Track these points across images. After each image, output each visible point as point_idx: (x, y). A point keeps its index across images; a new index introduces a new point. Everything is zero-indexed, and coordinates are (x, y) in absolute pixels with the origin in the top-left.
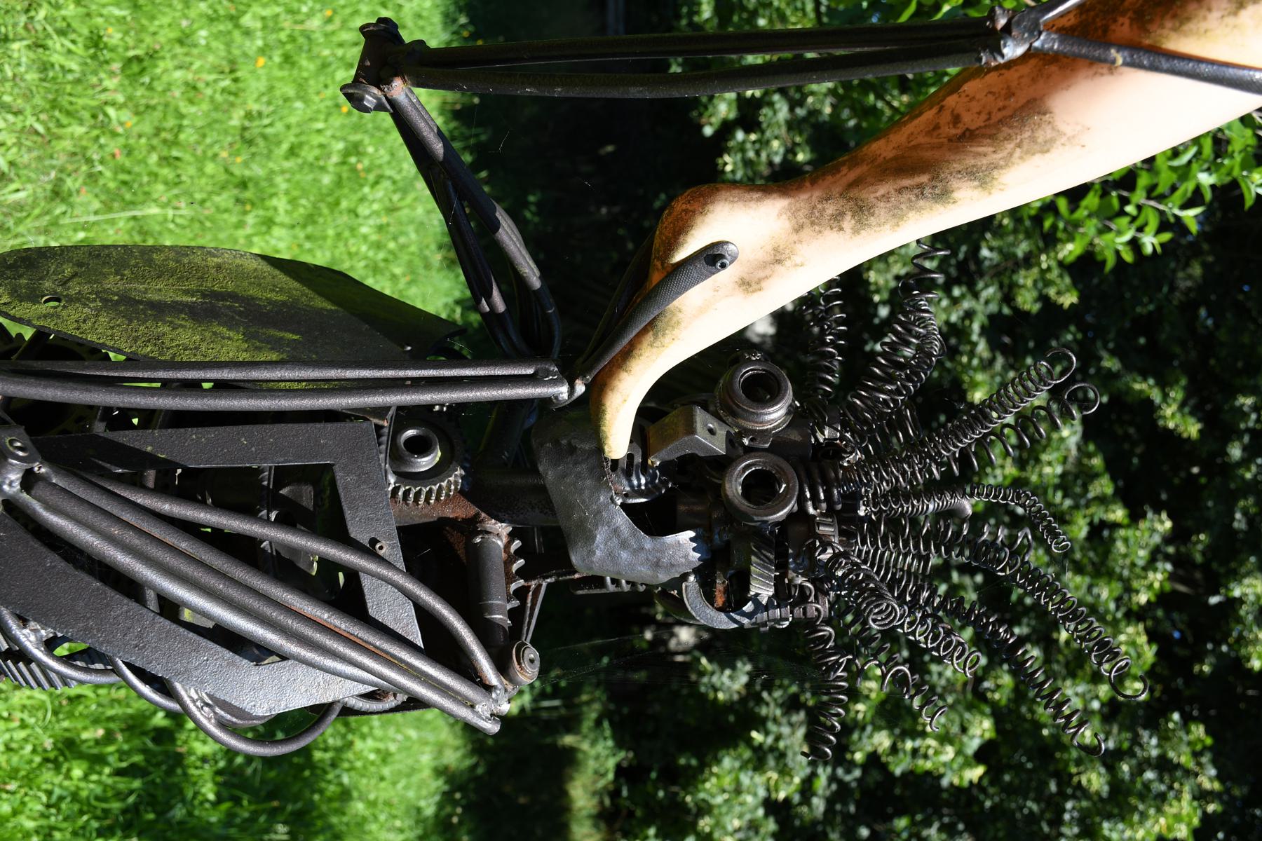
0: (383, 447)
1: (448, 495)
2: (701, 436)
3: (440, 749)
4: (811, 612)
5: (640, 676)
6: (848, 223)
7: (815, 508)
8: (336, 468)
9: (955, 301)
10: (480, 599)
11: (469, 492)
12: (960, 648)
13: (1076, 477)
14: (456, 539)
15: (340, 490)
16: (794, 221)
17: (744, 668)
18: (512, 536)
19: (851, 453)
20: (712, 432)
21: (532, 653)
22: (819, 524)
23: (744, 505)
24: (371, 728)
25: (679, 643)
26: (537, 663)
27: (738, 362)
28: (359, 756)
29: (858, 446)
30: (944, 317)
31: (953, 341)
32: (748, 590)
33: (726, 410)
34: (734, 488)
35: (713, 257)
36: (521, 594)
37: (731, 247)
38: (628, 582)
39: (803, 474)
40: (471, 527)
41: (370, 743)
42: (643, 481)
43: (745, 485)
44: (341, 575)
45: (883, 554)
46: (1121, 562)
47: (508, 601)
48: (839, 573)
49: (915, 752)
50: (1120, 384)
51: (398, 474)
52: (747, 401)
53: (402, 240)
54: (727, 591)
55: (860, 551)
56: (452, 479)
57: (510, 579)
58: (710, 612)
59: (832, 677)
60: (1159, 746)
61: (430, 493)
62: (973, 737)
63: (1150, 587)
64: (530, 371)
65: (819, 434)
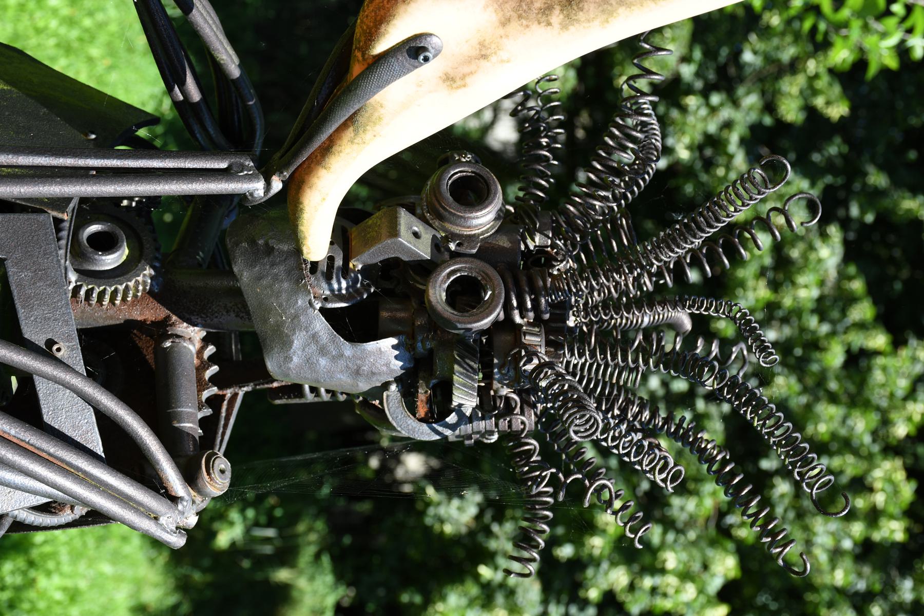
0: (63, 242)
1: (135, 296)
2: (405, 239)
3: (138, 584)
4: (517, 426)
5: (365, 507)
6: (556, 17)
7: (522, 317)
8: (8, 263)
9: (713, 110)
10: (170, 407)
11: (161, 293)
12: (662, 461)
13: (835, 300)
14: (144, 344)
15: (13, 287)
16: (500, 14)
17: (472, 501)
18: (206, 341)
19: (562, 261)
20: (416, 235)
21: (222, 463)
22: (525, 334)
23: (448, 312)
24: (58, 563)
25: (407, 472)
26: (228, 474)
27: (447, 162)
28: (43, 594)
29: (567, 254)
30: (700, 126)
31: (708, 152)
32: (451, 401)
33: (432, 213)
34: (437, 293)
35: (415, 50)
36: (214, 402)
37: (434, 40)
38: (328, 391)
39: (510, 281)
40: (160, 330)
41: (56, 580)
42: (344, 284)
44: (14, 379)
45: (591, 365)
46: (877, 390)
47: (200, 409)
48: (543, 384)
49: (654, 591)
50: (886, 203)
51: (82, 273)
52: (455, 204)
53: (100, 17)
54: (429, 401)
55: (568, 363)
56: (140, 279)
57: (202, 385)
58: (412, 422)
59: (534, 491)
60: (914, 589)
61: (115, 293)
62: (713, 575)
63: (909, 419)
64: (224, 165)
65: (529, 241)
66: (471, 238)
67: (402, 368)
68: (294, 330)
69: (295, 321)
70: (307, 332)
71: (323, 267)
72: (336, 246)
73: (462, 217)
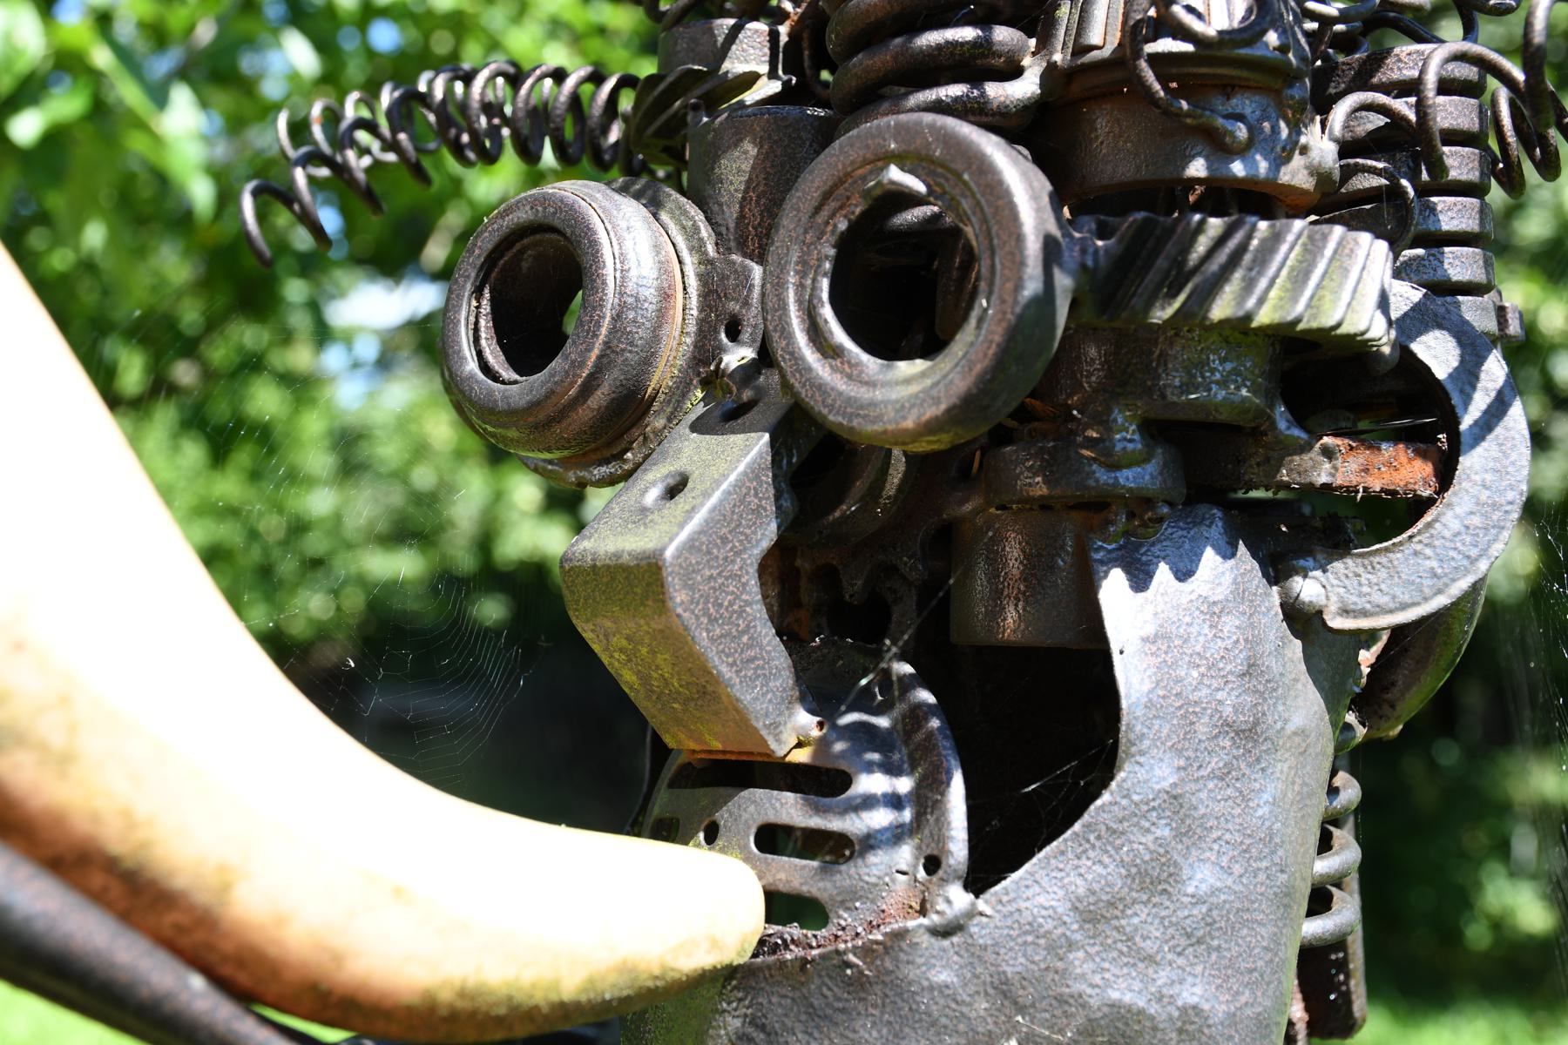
22: (1081, 49)
34: (897, 394)
42: (872, 783)
43: (888, 348)
58: (1453, 516)
66: (712, 293)
67: (1228, 553)
68: (1061, 1000)
69: (1026, 995)
70: (1071, 945)
71: (795, 873)
72: (722, 816)
73: (617, 318)
